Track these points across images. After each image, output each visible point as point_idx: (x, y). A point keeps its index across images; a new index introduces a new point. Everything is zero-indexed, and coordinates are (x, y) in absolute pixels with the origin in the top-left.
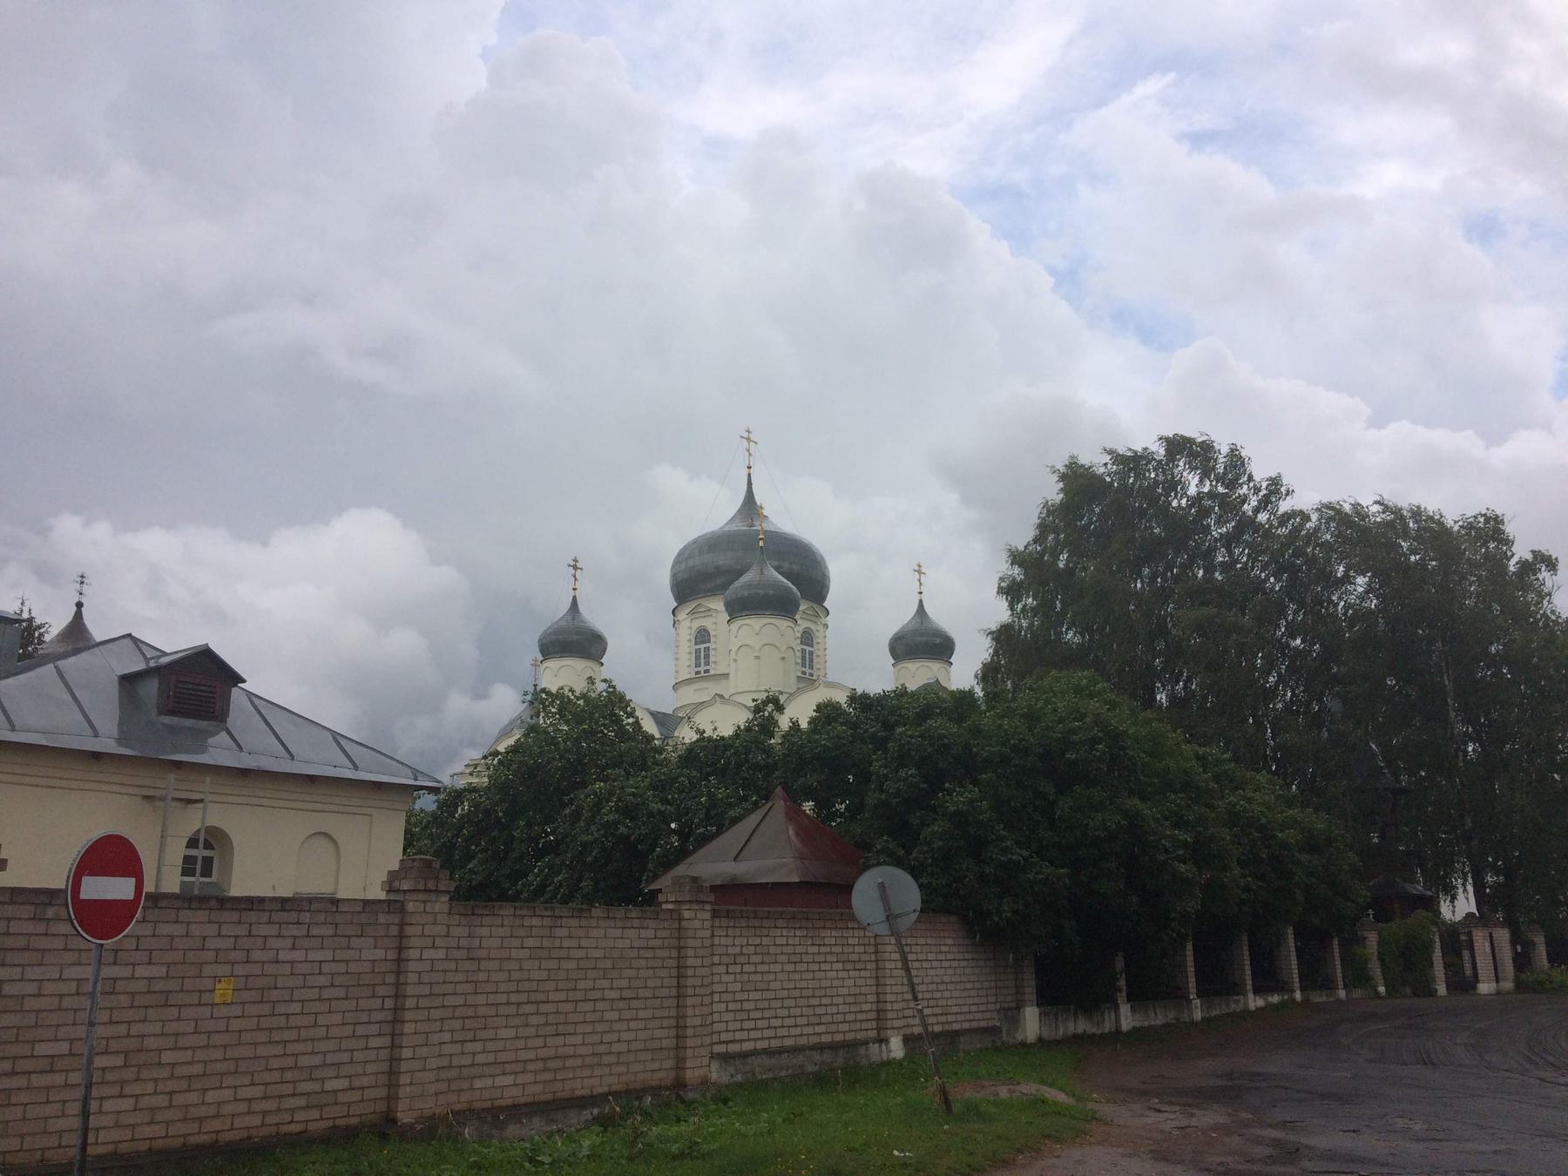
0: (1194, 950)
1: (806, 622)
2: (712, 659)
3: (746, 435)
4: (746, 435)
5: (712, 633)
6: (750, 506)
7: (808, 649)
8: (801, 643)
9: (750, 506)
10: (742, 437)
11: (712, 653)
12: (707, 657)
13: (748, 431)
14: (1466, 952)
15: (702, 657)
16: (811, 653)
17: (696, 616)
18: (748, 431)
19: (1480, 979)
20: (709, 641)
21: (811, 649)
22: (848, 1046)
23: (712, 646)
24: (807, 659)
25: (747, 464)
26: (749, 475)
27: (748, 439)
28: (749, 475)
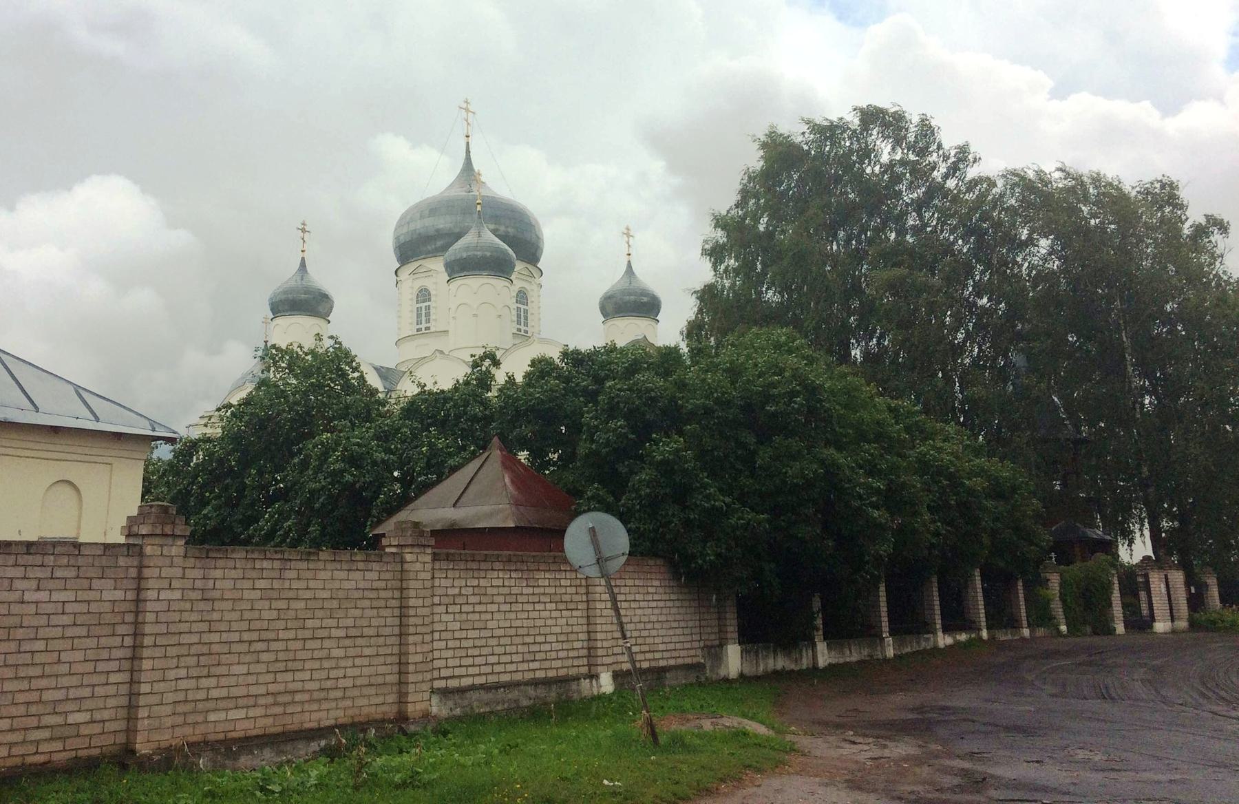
2: (432, 317)
3: (464, 106)
5: (433, 293)
7: (523, 307)
11: (432, 311)
12: (428, 315)
13: (467, 102)
15: (423, 314)
16: (526, 311)
18: (467, 102)
20: (430, 301)
23: (432, 304)
24: (522, 317)
26: (468, 143)
27: (467, 110)
28: (468, 143)
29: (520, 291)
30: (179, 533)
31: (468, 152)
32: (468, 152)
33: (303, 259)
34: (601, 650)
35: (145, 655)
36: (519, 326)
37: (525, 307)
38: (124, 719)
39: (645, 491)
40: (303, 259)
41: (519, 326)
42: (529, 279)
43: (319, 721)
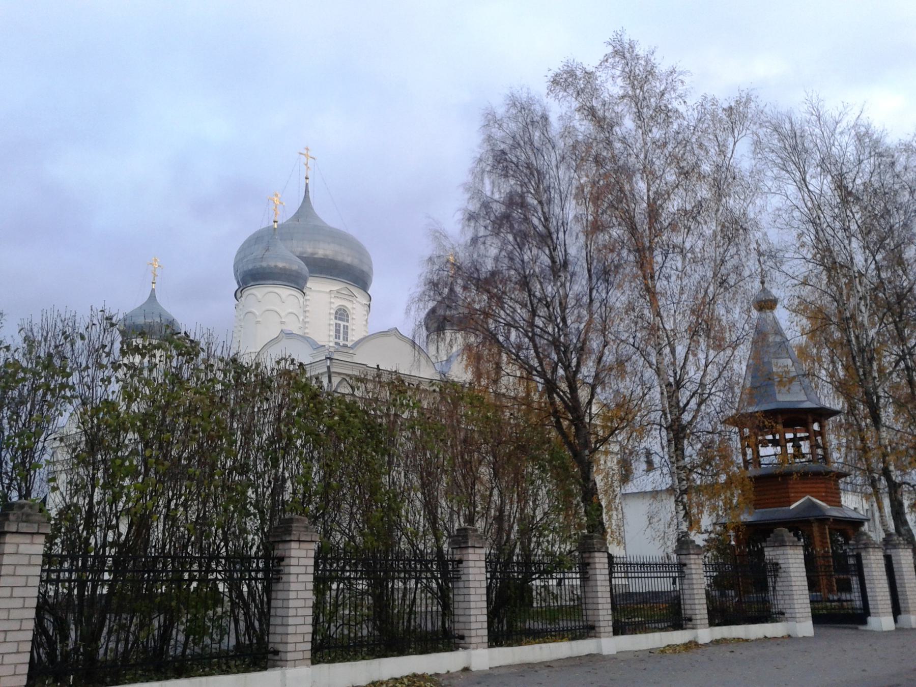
0: (709, 619)
1: (338, 300)
3: (305, 152)
4: (305, 152)
6: (152, 296)
7: (342, 323)
8: (336, 318)
9: (152, 296)
10: (300, 153)
13: (307, 149)
14: (854, 578)
16: (346, 327)
17: (339, 295)
18: (307, 149)
19: (871, 611)
21: (346, 324)
22: (316, 623)
24: (342, 331)
25: (152, 281)
26: (307, 185)
27: (307, 156)
28: (307, 185)
29: (340, 309)
30: (613, 583)
31: (307, 191)
32: (307, 191)
33: (153, 290)
34: (475, 624)
35: (289, 641)
36: (337, 340)
37: (346, 324)
38: (762, 457)
39: (295, 440)
40: (153, 290)
41: (337, 340)
42: (350, 298)
43: (781, 318)
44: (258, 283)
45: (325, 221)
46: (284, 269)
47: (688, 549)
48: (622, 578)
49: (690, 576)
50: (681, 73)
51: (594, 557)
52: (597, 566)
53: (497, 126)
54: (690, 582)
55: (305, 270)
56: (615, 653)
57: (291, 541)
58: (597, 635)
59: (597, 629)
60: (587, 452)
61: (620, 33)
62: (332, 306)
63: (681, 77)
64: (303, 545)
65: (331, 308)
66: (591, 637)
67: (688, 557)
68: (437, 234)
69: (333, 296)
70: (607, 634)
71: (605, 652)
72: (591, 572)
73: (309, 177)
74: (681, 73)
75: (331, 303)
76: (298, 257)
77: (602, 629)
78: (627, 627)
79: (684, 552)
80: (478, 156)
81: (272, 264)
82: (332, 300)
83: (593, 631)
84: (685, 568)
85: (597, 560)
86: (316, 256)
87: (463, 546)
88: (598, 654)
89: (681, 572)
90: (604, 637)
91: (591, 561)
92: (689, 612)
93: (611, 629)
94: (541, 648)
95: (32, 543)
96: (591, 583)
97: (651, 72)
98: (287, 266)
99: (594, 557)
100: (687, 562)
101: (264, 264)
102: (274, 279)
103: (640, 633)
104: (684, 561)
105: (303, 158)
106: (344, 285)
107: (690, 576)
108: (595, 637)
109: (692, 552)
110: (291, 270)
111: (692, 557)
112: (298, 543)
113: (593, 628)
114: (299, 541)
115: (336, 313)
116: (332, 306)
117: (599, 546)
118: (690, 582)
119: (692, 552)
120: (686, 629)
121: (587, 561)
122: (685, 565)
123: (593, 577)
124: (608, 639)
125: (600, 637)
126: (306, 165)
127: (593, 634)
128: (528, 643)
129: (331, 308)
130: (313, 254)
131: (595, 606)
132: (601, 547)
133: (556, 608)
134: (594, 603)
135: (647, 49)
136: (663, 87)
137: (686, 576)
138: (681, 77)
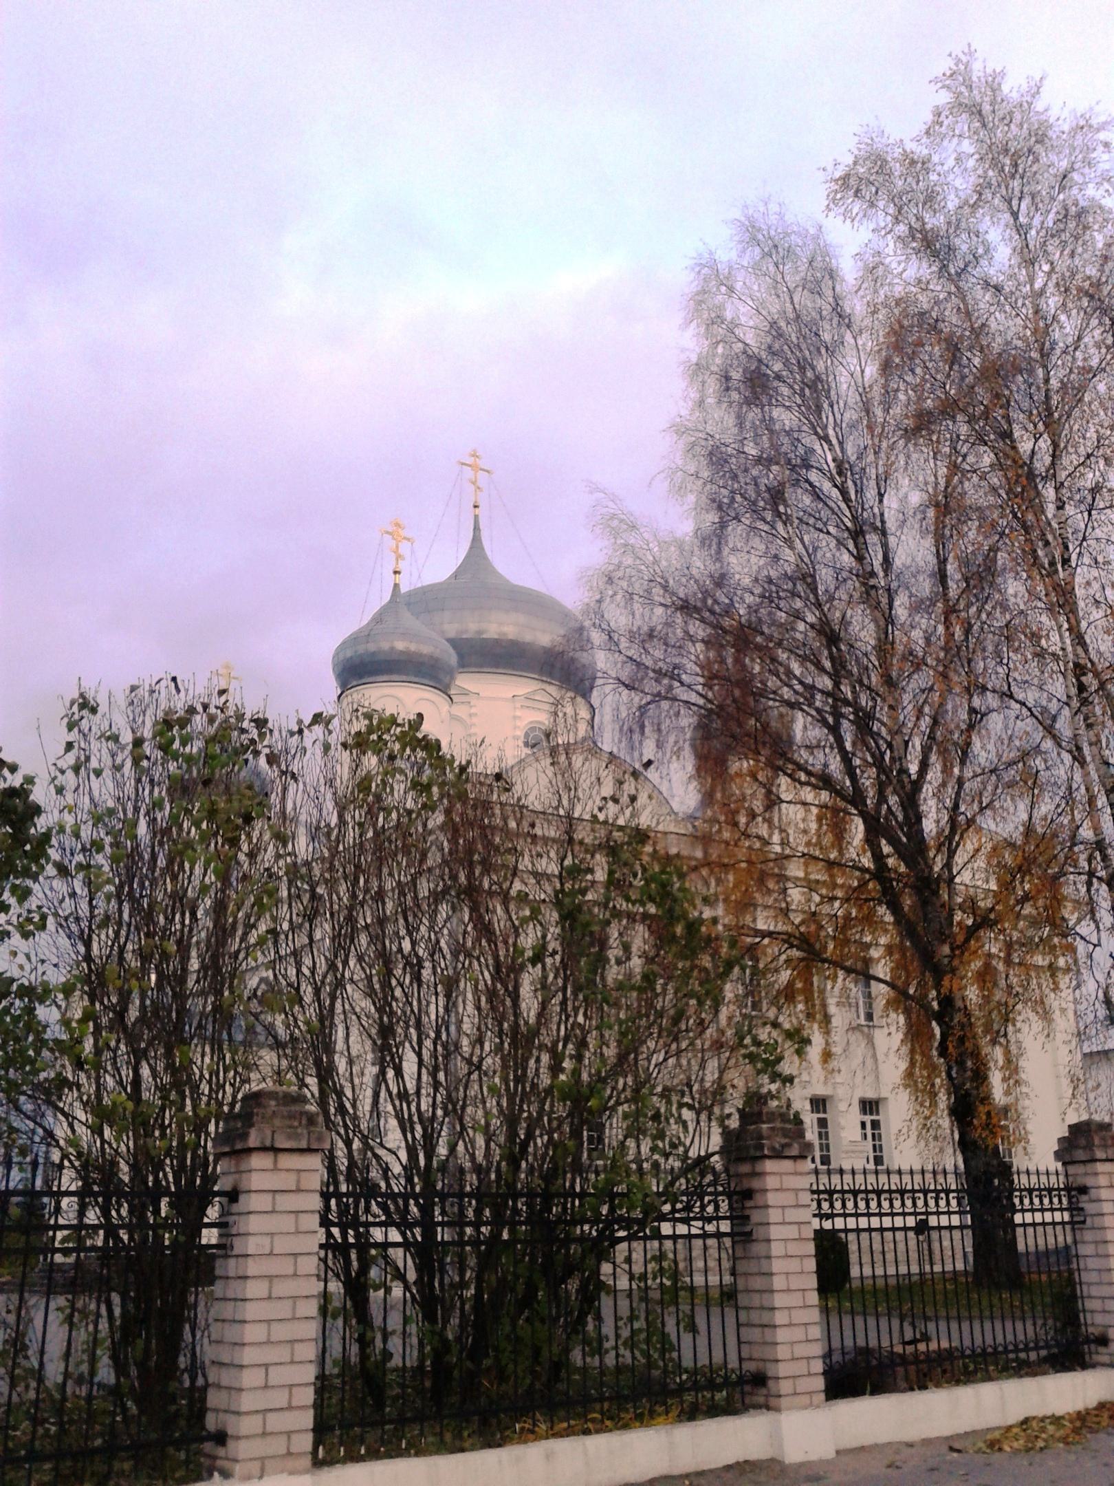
4: (470, 460)
13: (474, 455)
26: (476, 517)
27: (475, 468)
28: (476, 517)
31: (476, 528)
32: (476, 528)
44: (364, 681)
45: (507, 577)
46: (406, 653)
47: (1089, 1147)
48: (950, 1228)
49: (1097, 1221)
50: (1102, 127)
51: (762, 1174)
52: (772, 1198)
53: (723, 289)
54: (1098, 1236)
55: (453, 659)
56: (831, 1454)
57: (249, 1151)
58: (773, 1401)
59: (771, 1383)
60: (946, 950)
61: (964, 59)
62: (518, 723)
63: (1102, 136)
64: (287, 1161)
65: (515, 728)
66: (757, 1407)
67: (1090, 1168)
68: (615, 523)
69: (518, 705)
70: (805, 1400)
71: (793, 1455)
72: (756, 1216)
73: (479, 503)
74: (1102, 127)
75: (515, 718)
76: (449, 640)
77: (785, 1387)
78: (900, 1370)
79: (1080, 1155)
80: (694, 359)
81: (385, 646)
82: (518, 713)
83: (764, 1391)
84: (1084, 1198)
85: (771, 1182)
86: (484, 636)
87: (239, 1146)
88: (772, 1460)
89: (1074, 1208)
90: (789, 1409)
91: (755, 1184)
92: (1099, 1319)
93: (820, 1383)
94: (549, 1456)
95: (276, 1169)
96: (757, 1249)
97: (1041, 137)
98: (413, 647)
99: (762, 1174)
100: (1089, 1182)
101: (372, 647)
102: (399, 672)
103: (938, 1385)
104: (1081, 1181)
105: (469, 473)
106: (539, 685)
107: (1097, 1221)
108: (768, 1408)
109: (1100, 1154)
110: (421, 655)
111: (1100, 1167)
112: (271, 1155)
113: (760, 1380)
114: (275, 1150)
115: (527, 735)
116: (518, 723)
117: (779, 1141)
118: (1098, 1236)
119: (1100, 1154)
120: (1093, 1366)
121: (746, 1184)
122: (1083, 1190)
123: (759, 1233)
124: (807, 1414)
125: (777, 1410)
126: (474, 483)
127: (761, 1400)
128: (530, 1435)
129: (515, 728)
130: (480, 632)
131: (765, 1318)
132: (788, 1145)
133: (892, 1282)
134: (762, 1308)
135: (1025, 87)
136: (1064, 164)
137: (1089, 1220)
138: (1102, 136)
